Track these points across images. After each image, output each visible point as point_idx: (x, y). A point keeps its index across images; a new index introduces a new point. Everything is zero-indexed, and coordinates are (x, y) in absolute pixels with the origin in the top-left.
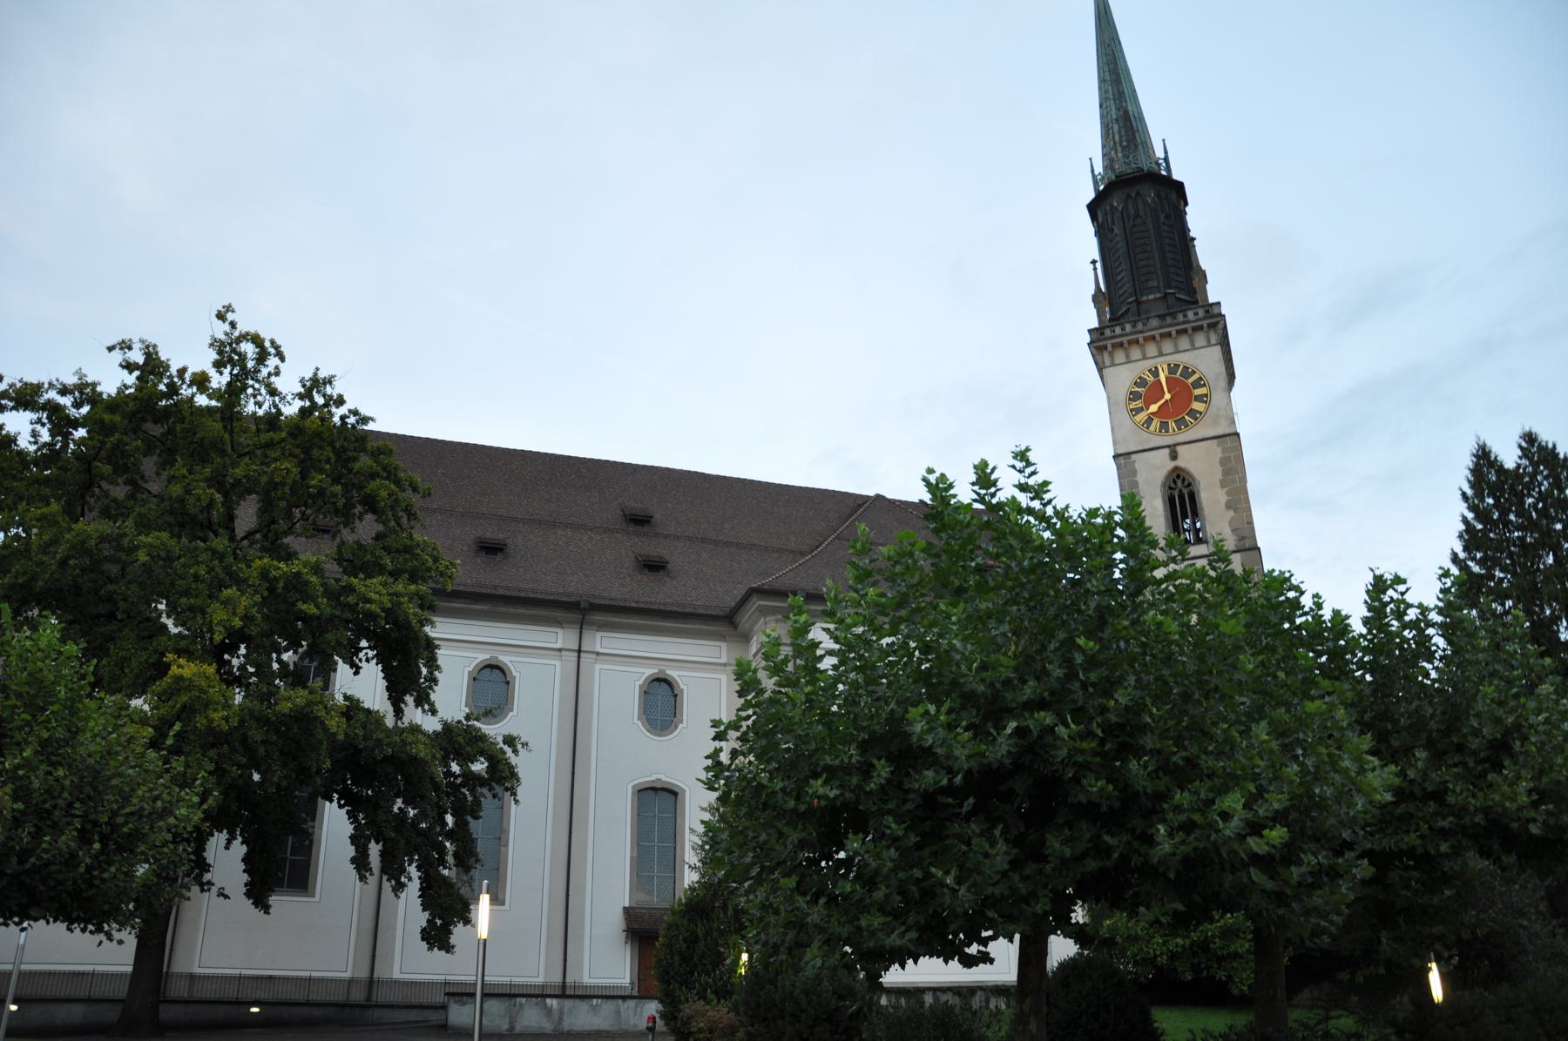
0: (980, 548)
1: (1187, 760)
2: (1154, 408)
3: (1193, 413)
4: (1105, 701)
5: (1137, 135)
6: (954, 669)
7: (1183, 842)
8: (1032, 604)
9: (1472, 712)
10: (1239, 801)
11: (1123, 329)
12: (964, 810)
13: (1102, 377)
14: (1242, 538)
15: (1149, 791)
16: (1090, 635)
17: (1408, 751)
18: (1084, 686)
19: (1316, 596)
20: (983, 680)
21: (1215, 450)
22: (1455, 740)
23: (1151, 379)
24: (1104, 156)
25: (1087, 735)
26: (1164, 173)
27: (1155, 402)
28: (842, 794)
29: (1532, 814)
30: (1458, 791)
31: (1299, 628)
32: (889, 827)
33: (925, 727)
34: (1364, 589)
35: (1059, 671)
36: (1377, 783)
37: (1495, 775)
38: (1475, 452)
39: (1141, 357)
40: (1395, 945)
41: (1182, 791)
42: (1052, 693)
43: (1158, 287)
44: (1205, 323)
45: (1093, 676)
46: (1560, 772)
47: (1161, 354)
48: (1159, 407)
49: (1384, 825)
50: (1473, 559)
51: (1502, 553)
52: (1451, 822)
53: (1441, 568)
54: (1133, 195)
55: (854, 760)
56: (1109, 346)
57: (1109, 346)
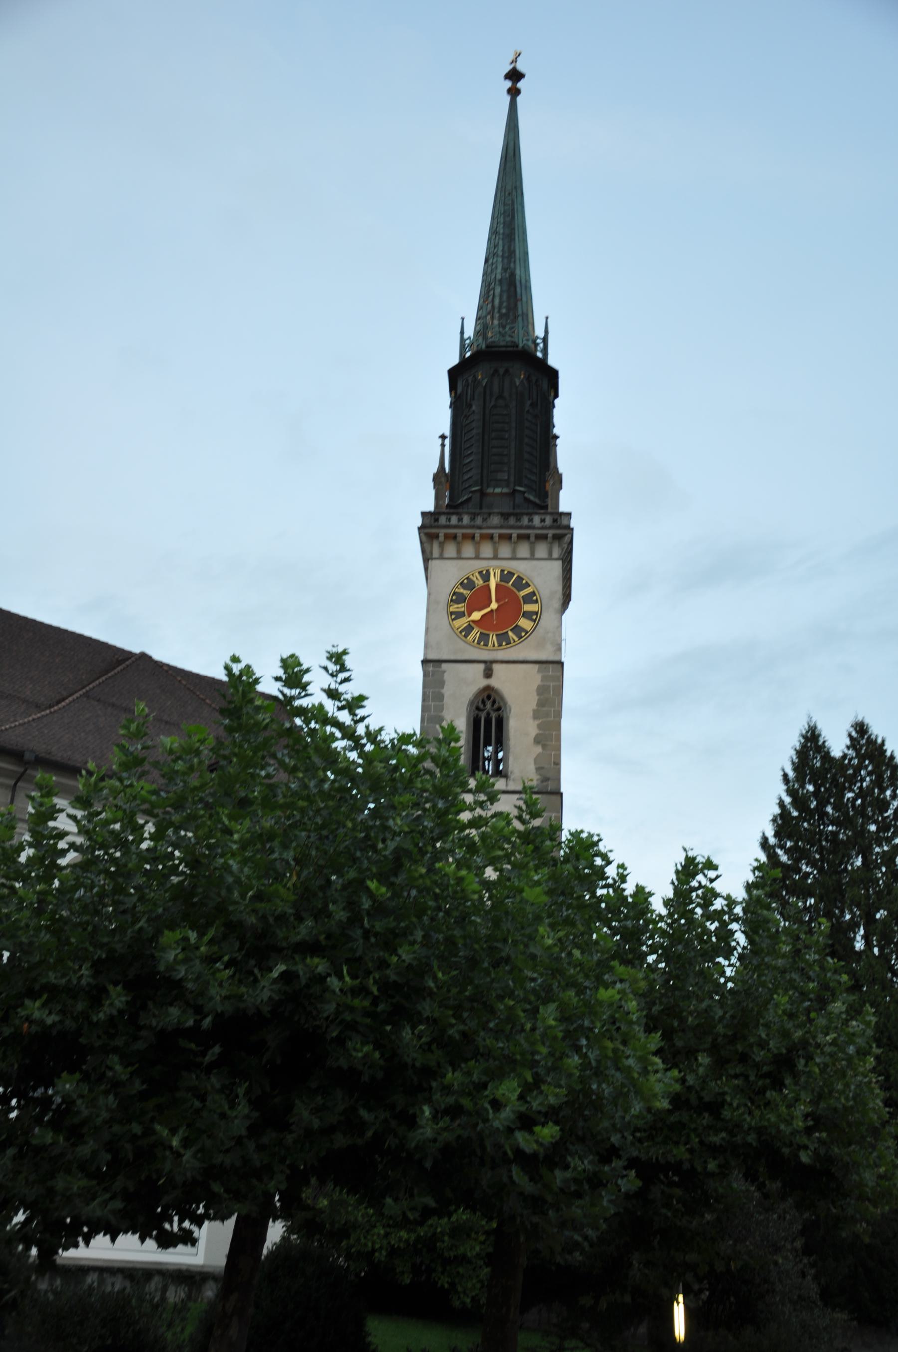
0: (274, 756)
1: (464, 1034)
2: (477, 615)
3: (518, 630)
4: (386, 955)
5: (519, 304)
6: (223, 892)
7: (446, 1129)
8: (325, 833)
9: (762, 1021)
10: (514, 1090)
11: (461, 520)
12: (208, 1058)
13: (426, 569)
14: (545, 779)
15: (418, 1064)
16: (382, 878)
17: (691, 1053)
18: (366, 934)
19: (622, 866)
20: (255, 911)
21: (533, 676)
22: (740, 1048)
23: (480, 582)
24: (478, 319)
25: (362, 991)
26: (539, 355)
27: (480, 609)
28: (61, 1022)
29: (805, 1141)
30: (735, 1104)
31: (600, 899)
32: (111, 1068)
33: (180, 957)
34: (674, 869)
35: (342, 913)
36: (658, 1088)
37: (774, 1093)
38: (804, 732)
39: (473, 556)
40: (646, 1271)
41: (454, 1071)
42: (329, 937)
43: (508, 481)
44: (550, 533)
45: (379, 926)
46: (838, 1099)
47: (496, 557)
48: (483, 616)
49: (654, 1132)
50: (782, 847)
51: (813, 845)
52: (723, 1139)
53: (757, 860)
54: (502, 371)
55: (84, 982)
56: (441, 536)
57: (441, 536)
